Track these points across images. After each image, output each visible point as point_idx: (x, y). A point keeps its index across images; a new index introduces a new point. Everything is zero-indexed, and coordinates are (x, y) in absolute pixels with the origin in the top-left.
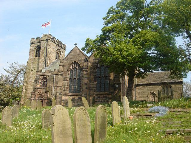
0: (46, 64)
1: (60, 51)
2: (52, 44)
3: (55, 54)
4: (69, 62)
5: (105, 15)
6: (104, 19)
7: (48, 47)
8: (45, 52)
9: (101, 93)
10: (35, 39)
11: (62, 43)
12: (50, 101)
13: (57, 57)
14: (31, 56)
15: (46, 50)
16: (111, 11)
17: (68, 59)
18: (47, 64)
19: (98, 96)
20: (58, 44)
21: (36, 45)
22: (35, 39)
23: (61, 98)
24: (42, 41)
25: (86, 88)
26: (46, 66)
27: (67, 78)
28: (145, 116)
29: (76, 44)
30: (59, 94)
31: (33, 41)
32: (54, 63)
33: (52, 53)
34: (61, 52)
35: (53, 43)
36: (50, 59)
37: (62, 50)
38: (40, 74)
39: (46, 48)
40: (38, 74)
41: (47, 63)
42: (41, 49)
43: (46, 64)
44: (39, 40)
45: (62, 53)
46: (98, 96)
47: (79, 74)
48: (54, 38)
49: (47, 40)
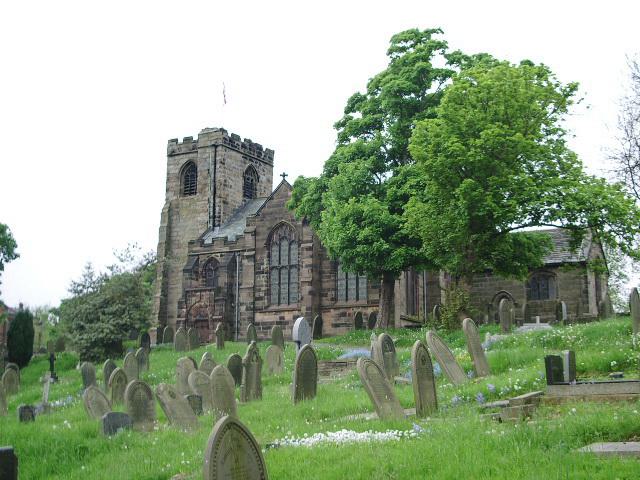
0: (214, 217)
1: (255, 172)
2: (230, 157)
3: (241, 182)
4: (268, 224)
5: (340, 116)
6: (338, 125)
7: (218, 166)
8: (209, 181)
9: (357, 310)
10: (181, 141)
11: (259, 148)
12: (228, 325)
13: (249, 191)
14: (171, 194)
15: (212, 176)
16: (355, 103)
17: (264, 215)
18: (219, 217)
19: (341, 311)
20: (246, 152)
21: (184, 160)
22: (181, 141)
23: (252, 319)
24: (199, 151)
25: (310, 293)
26: (217, 224)
27: (265, 266)
28: (606, 436)
29: (284, 175)
30: (247, 309)
31: (175, 148)
32: (238, 211)
33: (231, 183)
34: (261, 173)
35: (234, 153)
36: (224, 202)
37: (260, 168)
38: (198, 248)
39: (212, 170)
40: (194, 249)
41: (217, 214)
42: (199, 174)
43: (214, 217)
44: (191, 146)
45: (263, 178)
46: (341, 311)
47: (525, 235)
48: (235, 137)
49: (215, 146)
